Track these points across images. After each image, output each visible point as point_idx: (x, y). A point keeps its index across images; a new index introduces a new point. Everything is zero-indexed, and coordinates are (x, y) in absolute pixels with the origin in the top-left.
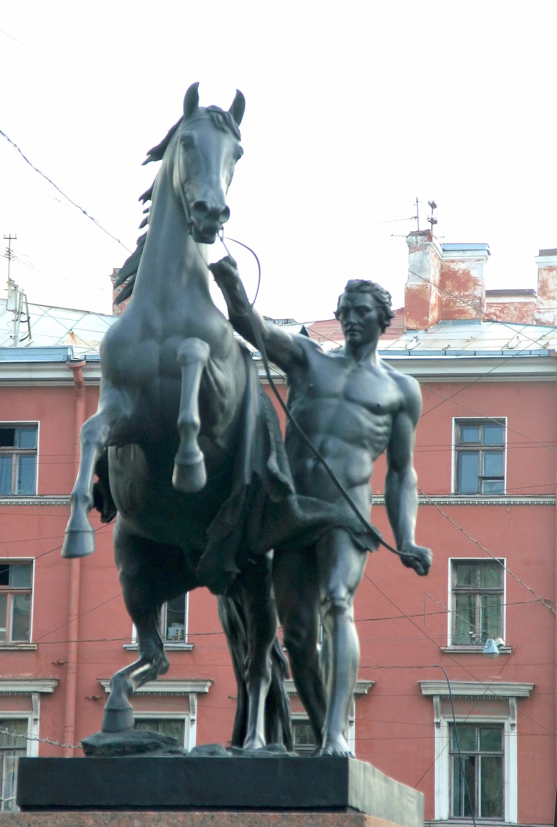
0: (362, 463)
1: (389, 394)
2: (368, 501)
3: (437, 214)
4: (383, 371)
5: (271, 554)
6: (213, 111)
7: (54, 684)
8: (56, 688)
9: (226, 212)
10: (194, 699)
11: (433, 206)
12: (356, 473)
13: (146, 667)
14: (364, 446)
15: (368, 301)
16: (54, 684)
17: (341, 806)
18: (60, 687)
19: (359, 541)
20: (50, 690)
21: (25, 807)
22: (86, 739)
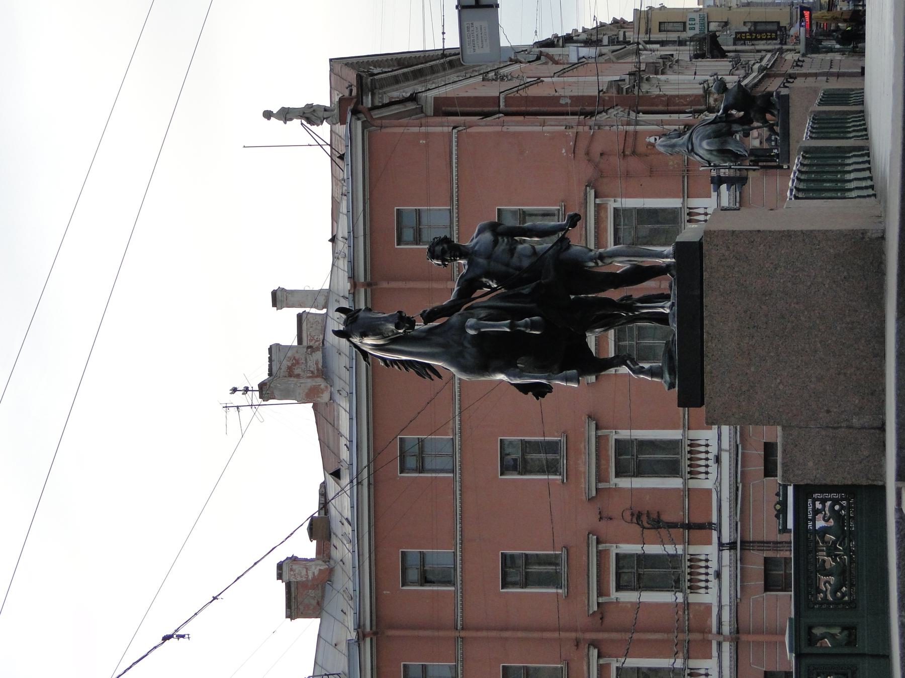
0: (525, 248)
1: (488, 236)
2: (543, 245)
3: (241, 387)
4: (475, 241)
5: (572, 297)
6: (346, 323)
7: (592, 648)
8: (595, 648)
9: (400, 312)
10: (601, 547)
11: (235, 390)
12: (529, 251)
13: (628, 362)
14: (515, 248)
15: (438, 249)
16: (592, 648)
17: (700, 244)
18: (593, 644)
19: (564, 247)
20: (596, 651)
21: (702, 404)
22: (666, 388)
